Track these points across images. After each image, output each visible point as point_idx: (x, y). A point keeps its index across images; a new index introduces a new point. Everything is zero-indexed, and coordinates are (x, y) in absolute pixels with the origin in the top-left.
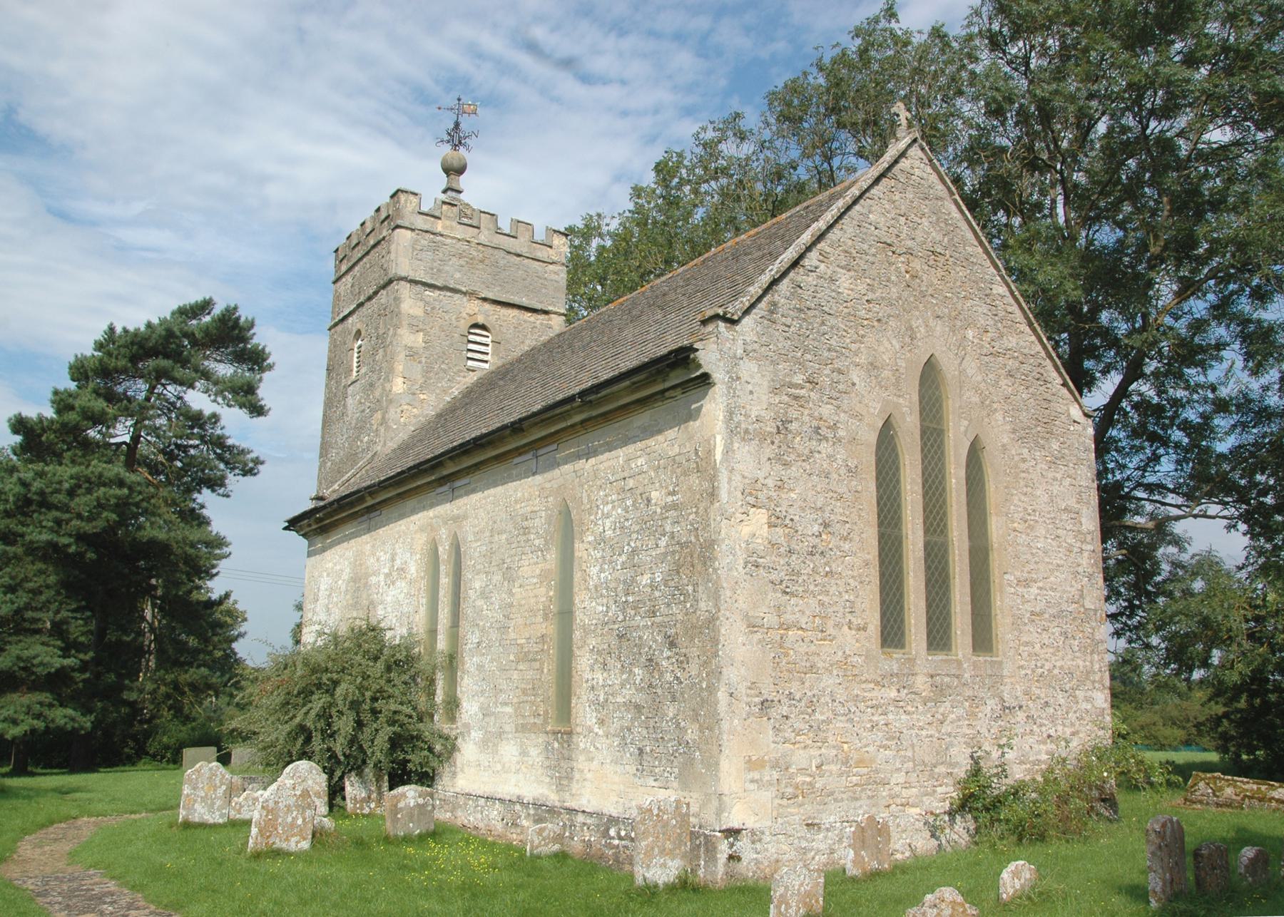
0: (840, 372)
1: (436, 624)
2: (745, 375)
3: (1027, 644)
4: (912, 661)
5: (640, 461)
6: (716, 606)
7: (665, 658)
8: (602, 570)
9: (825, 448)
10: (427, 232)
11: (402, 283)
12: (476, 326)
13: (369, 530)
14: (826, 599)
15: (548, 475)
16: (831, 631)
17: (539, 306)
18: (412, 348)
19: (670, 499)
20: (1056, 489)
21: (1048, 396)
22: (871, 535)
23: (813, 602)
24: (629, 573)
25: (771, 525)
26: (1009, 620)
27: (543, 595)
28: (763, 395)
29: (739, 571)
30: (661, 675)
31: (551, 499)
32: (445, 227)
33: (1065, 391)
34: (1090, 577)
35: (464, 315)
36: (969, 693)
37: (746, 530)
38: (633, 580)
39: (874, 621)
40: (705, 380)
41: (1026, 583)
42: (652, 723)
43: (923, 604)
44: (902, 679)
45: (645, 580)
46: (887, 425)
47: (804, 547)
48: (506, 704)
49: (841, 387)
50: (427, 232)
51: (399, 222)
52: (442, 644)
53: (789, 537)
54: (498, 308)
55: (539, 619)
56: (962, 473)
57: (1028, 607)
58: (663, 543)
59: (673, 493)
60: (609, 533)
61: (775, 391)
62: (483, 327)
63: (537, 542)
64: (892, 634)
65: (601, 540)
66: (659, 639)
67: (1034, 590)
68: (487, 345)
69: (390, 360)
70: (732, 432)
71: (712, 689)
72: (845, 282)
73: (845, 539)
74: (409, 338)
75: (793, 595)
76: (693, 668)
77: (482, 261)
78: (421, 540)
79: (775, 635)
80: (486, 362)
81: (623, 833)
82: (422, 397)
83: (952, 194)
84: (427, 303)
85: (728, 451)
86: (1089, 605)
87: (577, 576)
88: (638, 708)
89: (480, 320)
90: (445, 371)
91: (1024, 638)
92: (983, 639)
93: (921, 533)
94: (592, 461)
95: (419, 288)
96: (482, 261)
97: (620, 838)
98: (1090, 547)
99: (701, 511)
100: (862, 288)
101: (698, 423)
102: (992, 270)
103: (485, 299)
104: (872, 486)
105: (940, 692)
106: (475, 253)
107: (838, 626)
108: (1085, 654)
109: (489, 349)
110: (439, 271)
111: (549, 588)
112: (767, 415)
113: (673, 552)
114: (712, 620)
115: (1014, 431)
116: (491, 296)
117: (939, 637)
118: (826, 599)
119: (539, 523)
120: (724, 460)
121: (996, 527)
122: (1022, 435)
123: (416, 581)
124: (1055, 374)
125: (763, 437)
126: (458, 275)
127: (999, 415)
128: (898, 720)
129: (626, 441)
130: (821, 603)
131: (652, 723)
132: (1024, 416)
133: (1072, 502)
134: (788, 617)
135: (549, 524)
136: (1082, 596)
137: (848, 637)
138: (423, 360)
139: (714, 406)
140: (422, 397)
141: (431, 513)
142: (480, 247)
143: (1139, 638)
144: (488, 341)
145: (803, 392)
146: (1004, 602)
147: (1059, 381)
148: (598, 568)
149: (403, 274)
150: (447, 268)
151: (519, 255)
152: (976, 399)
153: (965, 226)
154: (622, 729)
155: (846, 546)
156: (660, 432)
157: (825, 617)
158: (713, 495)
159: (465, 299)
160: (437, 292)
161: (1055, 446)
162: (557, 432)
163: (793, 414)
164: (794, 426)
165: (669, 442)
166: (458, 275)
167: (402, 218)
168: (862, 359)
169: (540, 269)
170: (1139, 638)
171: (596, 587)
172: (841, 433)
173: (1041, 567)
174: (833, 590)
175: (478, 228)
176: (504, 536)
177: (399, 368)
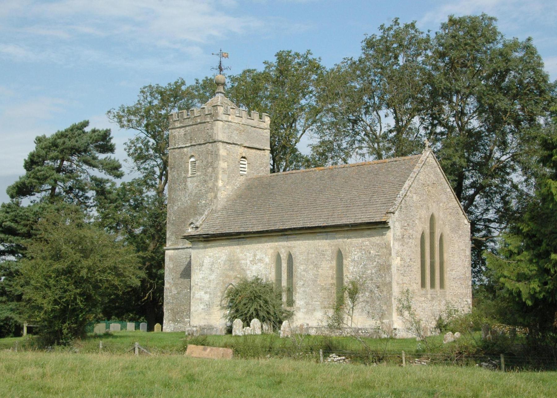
0: (414, 221)
1: (281, 277)
2: (396, 226)
3: (452, 286)
4: (427, 291)
5: (367, 243)
6: (391, 279)
7: (376, 291)
8: (354, 268)
9: (411, 240)
10: (226, 121)
11: (220, 143)
12: (243, 157)
13: (238, 245)
14: (410, 277)
15: (333, 241)
16: (412, 284)
17: (262, 148)
18: (223, 168)
19: (377, 253)
20: (460, 244)
21: (459, 218)
22: (419, 260)
23: (408, 278)
24: (364, 270)
25: (401, 260)
26: (448, 280)
27: (332, 272)
28: (400, 230)
29: (396, 271)
30: (375, 294)
31: (333, 247)
32: (232, 119)
33: (463, 216)
34: (468, 268)
35: (239, 154)
36: (439, 299)
37: (396, 262)
38: (365, 272)
39: (419, 281)
40: (389, 228)
41: (452, 270)
42: (372, 305)
43: (429, 277)
44: (425, 295)
45: (369, 272)
46: (423, 233)
47: (406, 265)
48: (316, 301)
49: (414, 225)
50: (226, 121)
51: (218, 118)
52: (284, 283)
53: (404, 263)
54: (249, 150)
55: (330, 279)
56: (438, 243)
57: (452, 277)
58: (375, 263)
59: (378, 252)
60: (356, 259)
61: (401, 229)
62: (244, 158)
63: (328, 258)
64: (423, 285)
65: (353, 260)
66: (374, 286)
67: (454, 272)
68: (245, 165)
69: (217, 174)
70: (394, 240)
71: (390, 298)
72: (415, 197)
73: (414, 262)
74: (223, 165)
75: (405, 276)
76: (385, 293)
77: (243, 131)
78: (271, 251)
79: (401, 286)
80: (245, 171)
81: (363, 332)
82: (228, 187)
83: (438, 165)
84: (228, 150)
85: (393, 244)
86: (467, 276)
87: (345, 269)
88: (367, 302)
89: (244, 155)
90: (234, 176)
91: (451, 285)
92: (442, 286)
93: (429, 259)
94: (349, 240)
95: (225, 144)
96: (243, 131)
97: (362, 333)
98: (468, 260)
99: (387, 257)
100: (418, 198)
101: (385, 237)
102: (447, 185)
103: (245, 147)
104: (420, 249)
105: (433, 298)
106: (241, 128)
107: (413, 283)
108: (466, 289)
109: (246, 166)
110: (231, 137)
111: (333, 270)
112: (400, 234)
113: (378, 266)
114: (390, 283)
115: (450, 230)
116: (247, 146)
117: (433, 285)
118: (410, 277)
119: (329, 253)
120: (393, 246)
121: (445, 256)
122: (453, 230)
123: (269, 264)
124: (461, 212)
125: (399, 240)
126: (236, 138)
127: (447, 226)
128: (424, 305)
129: (362, 237)
130: (410, 278)
131: (372, 305)
132: (453, 225)
133: (464, 248)
134: (404, 281)
135: (333, 254)
136: (465, 273)
137: (415, 285)
138: (227, 173)
139: (390, 234)
140: (228, 187)
141: (276, 244)
142: (243, 125)
143: (477, 276)
144: (246, 163)
145: (406, 228)
146: (447, 276)
147: (462, 213)
148: (352, 267)
149: (220, 139)
150: (233, 135)
151: (255, 127)
152: (442, 223)
153: (441, 174)
154: (362, 307)
155: (414, 264)
156: (374, 236)
157: (410, 281)
158: (390, 254)
159: (239, 147)
160: (230, 145)
161: (460, 232)
162: (337, 231)
163: (405, 233)
164: (405, 236)
165: (376, 239)
166: (236, 138)
167: (218, 116)
168: (418, 217)
169: (261, 132)
170: (477, 276)
171: (352, 272)
172: (414, 236)
173: (456, 266)
174: (412, 275)
175: (242, 117)
176: (314, 255)
177: (220, 176)
